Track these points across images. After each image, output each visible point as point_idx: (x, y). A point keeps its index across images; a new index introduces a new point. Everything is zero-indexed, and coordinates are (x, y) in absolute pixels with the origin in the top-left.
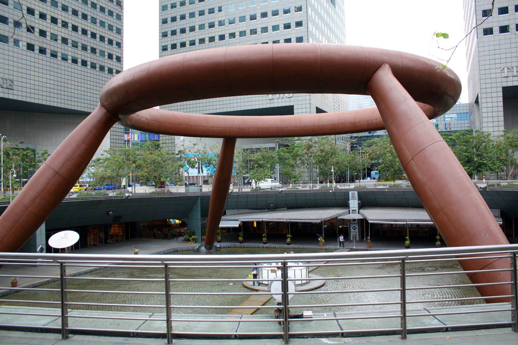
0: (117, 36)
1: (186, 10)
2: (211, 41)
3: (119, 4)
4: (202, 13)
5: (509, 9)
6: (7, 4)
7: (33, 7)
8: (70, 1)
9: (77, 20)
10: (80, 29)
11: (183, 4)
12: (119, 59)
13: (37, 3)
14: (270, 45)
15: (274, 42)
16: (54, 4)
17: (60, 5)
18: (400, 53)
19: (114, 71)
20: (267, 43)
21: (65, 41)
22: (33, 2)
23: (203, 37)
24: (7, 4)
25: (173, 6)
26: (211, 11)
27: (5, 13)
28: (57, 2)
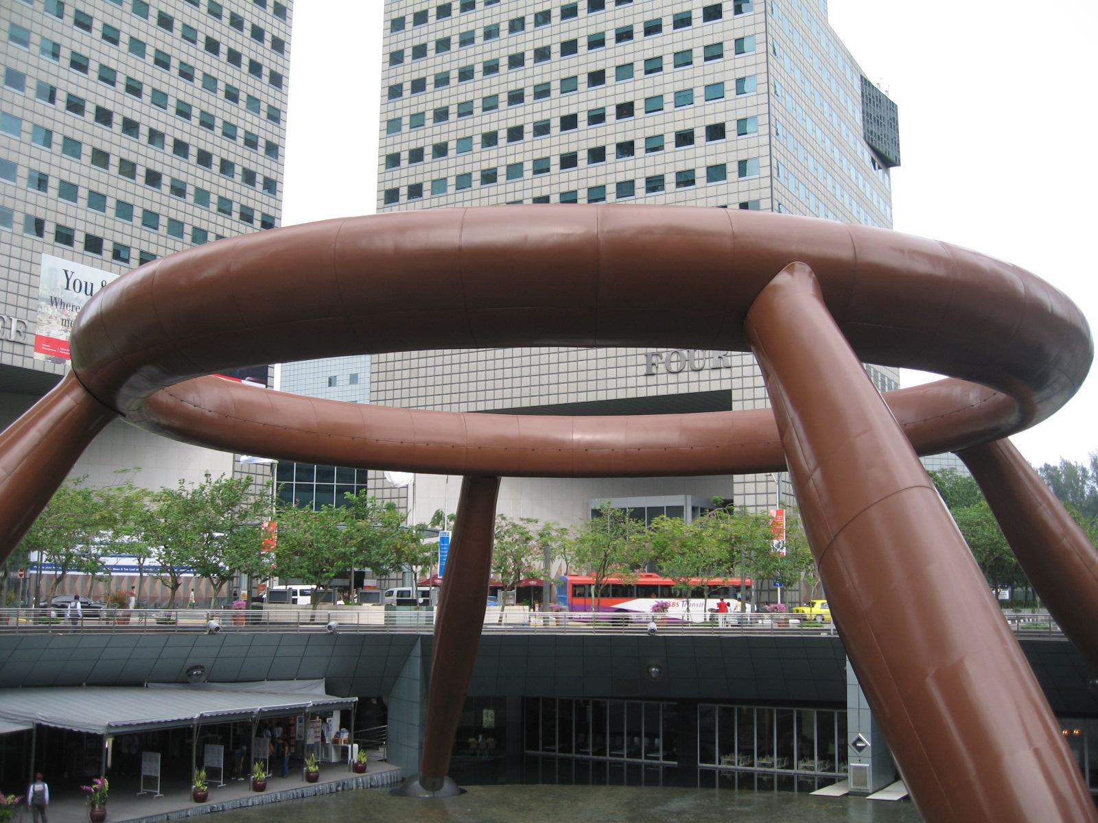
0: (272, 91)
1: (459, 23)
2: (489, 145)
3: (281, 11)
4: (624, 35)
5: (727, 129)
6: (197, 5)
7: (170, 12)
8: (172, 3)
9: (168, 39)
10: (245, 61)
11: (444, 11)
12: (271, 186)
13: (179, 6)
14: (529, 208)
15: (744, 206)
16: (141, 8)
17: (153, 12)
18: (196, 692)
19: (135, 254)
20: (520, 202)
21: (134, 89)
22: (242, 3)
23: (688, 125)
24: (197, 5)
25: (421, 18)
26: (653, 28)
27: (124, 24)
28: (147, 5)
